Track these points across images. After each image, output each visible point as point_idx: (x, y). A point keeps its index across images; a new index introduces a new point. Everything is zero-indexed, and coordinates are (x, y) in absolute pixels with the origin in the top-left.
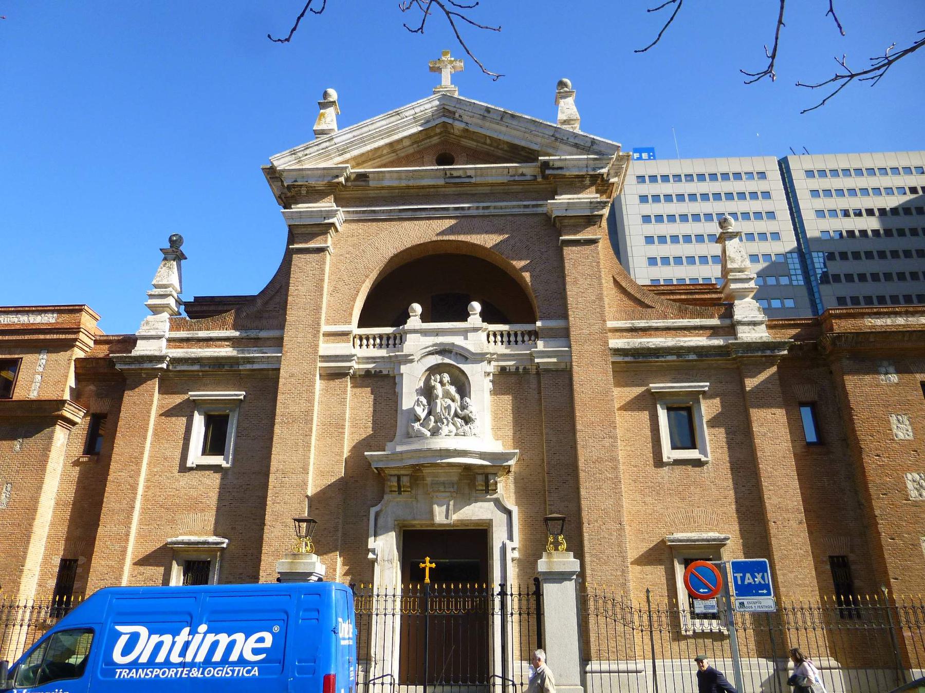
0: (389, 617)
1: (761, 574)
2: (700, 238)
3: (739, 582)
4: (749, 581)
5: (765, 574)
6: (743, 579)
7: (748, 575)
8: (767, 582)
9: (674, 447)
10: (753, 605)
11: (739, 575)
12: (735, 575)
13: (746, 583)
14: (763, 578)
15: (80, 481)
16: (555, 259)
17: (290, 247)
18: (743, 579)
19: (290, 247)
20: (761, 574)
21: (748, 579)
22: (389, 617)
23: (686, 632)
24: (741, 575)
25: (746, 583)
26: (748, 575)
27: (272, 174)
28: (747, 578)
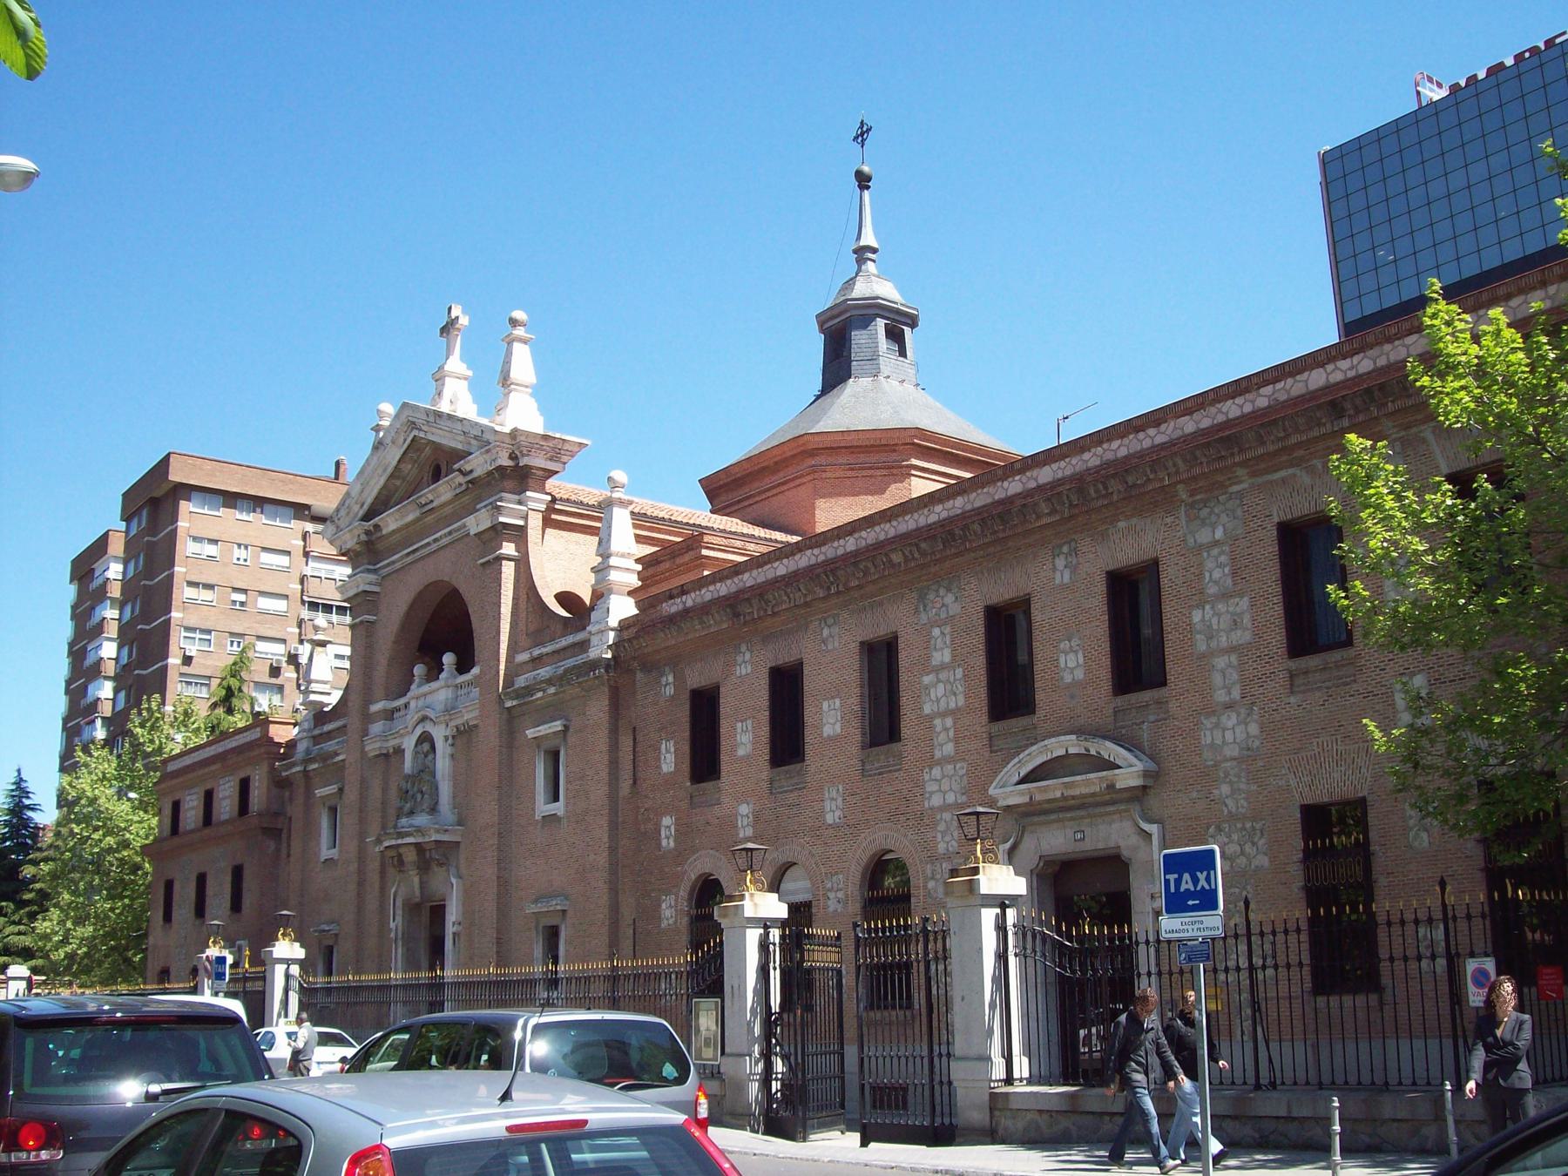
0: (1397, 953)
1: (1205, 873)
2: (1545, 1071)
3: (1173, 890)
4: (1187, 887)
5: (1212, 872)
6: (1178, 882)
7: (1186, 876)
8: (1213, 887)
9: (1212, 852)
10: (1190, 928)
11: (1172, 877)
12: (1167, 877)
13: (1182, 890)
14: (1208, 879)
15: (831, 495)
16: (895, 607)
17: (543, 1146)
18: (1178, 882)
19: (543, 1146)
20: (1205, 873)
21: (1187, 884)
22: (1397, 953)
23: (1210, 638)
24: (1176, 876)
25: (1182, 890)
26: (1186, 876)
27: (610, 479)
28: (1184, 882)
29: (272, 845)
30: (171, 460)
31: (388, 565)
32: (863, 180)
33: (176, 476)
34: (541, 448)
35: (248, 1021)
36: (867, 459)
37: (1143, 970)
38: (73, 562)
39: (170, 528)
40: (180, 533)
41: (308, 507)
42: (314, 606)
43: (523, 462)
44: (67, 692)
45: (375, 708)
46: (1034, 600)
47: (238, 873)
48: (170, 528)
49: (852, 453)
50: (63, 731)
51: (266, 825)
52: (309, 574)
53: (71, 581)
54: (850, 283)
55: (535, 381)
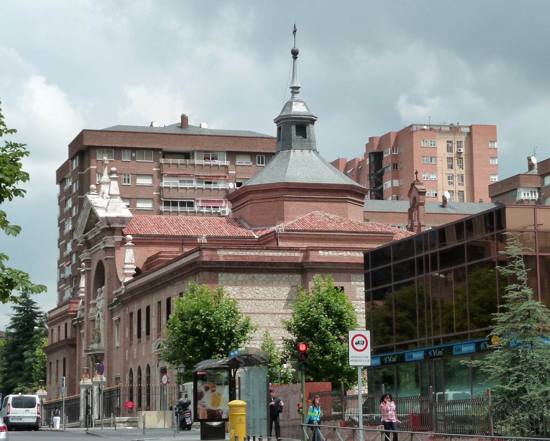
29: (73, 350)
30: (84, 134)
31: (96, 248)
32: (295, 54)
33: (87, 142)
34: (117, 221)
35: (207, 425)
36: (264, 196)
37: (176, 395)
38: (56, 171)
39: (88, 169)
40: (93, 172)
41: (160, 149)
42: (167, 204)
43: (112, 226)
44: (59, 247)
45: (91, 302)
46: (133, 313)
47: (64, 360)
48: (88, 169)
49: (263, 192)
50: (58, 268)
51: (70, 343)
52: (164, 185)
53: (57, 184)
54: (289, 105)
55: (119, 193)
